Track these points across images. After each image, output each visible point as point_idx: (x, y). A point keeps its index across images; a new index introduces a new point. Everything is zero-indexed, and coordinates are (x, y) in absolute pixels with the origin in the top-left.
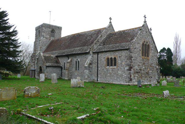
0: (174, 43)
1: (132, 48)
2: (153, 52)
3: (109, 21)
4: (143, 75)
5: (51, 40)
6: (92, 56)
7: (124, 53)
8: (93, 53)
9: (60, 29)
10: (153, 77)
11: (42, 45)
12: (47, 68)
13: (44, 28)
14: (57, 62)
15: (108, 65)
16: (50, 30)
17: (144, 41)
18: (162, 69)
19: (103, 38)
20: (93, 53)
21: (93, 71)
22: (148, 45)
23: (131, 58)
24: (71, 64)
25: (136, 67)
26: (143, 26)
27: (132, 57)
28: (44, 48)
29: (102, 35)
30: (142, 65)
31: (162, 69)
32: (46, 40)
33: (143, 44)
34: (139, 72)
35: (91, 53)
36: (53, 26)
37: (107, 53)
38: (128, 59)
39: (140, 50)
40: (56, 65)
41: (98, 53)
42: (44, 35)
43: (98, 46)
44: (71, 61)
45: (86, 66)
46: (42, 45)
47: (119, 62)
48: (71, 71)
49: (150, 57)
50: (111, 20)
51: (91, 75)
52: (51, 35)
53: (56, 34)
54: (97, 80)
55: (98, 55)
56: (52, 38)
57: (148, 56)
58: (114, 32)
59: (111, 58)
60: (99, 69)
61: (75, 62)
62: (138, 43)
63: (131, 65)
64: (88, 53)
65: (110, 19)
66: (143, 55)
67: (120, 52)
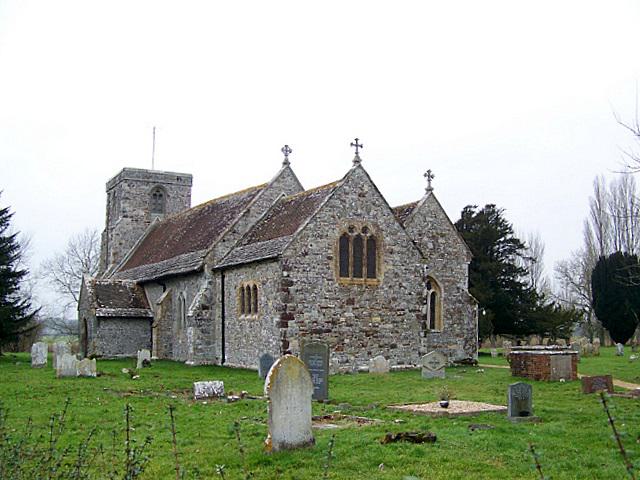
0: (588, 234)
1: (288, 253)
2: (397, 258)
3: (282, 158)
4: (347, 341)
5: (153, 223)
6: (210, 283)
7: (272, 272)
8: (215, 271)
9: (185, 181)
10: (400, 346)
11: (120, 244)
12: (99, 325)
13: (125, 185)
14: (139, 303)
15: (243, 312)
16: (148, 188)
17: (351, 229)
18: (484, 313)
19: (253, 221)
20: (215, 271)
21: (214, 331)
22: (373, 240)
23: (287, 284)
24: (167, 310)
25: (311, 315)
26: (282, 175)
27: (292, 284)
28: (128, 253)
29: (249, 211)
30: (341, 307)
31: (484, 313)
32: (140, 220)
33: (344, 239)
34: (329, 331)
35: (207, 271)
36: (157, 175)
37: (243, 270)
38: (278, 291)
39: (330, 258)
40: (132, 311)
41: (222, 271)
42: (127, 209)
43: (232, 249)
44: (169, 298)
45: (190, 314)
46: (120, 244)
47: (263, 299)
48: (169, 333)
49: (381, 278)
50: (433, 181)
51: (208, 343)
52: (153, 207)
53: (169, 203)
54: (223, 360)
55: (223, 277)
56: (157, 218)
57: (372, 274)
58: (302, 197)
59: (248, 287)
60: (227, 322)
61: (177, 302)
62: (321, 237)
63: (285, 310)
64: (199, 273)
65: (429, 176)
66: (343, 272)
67: (264, 267)
